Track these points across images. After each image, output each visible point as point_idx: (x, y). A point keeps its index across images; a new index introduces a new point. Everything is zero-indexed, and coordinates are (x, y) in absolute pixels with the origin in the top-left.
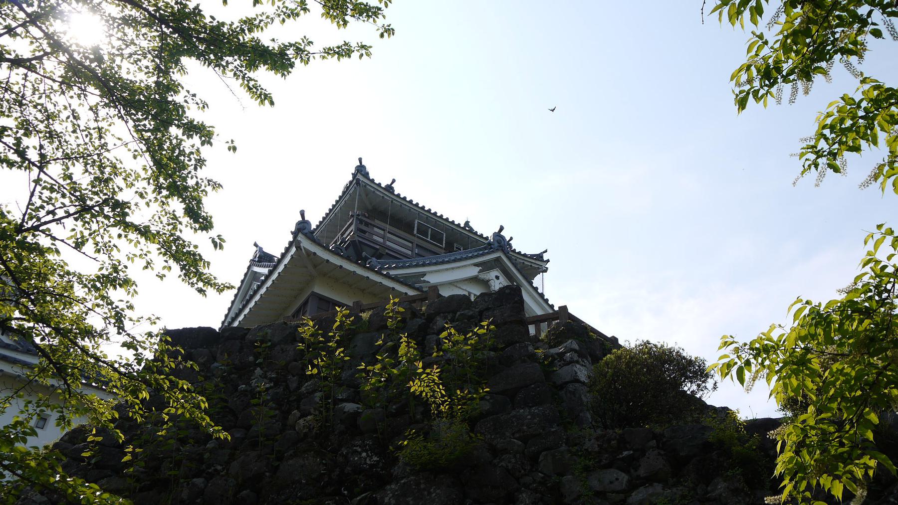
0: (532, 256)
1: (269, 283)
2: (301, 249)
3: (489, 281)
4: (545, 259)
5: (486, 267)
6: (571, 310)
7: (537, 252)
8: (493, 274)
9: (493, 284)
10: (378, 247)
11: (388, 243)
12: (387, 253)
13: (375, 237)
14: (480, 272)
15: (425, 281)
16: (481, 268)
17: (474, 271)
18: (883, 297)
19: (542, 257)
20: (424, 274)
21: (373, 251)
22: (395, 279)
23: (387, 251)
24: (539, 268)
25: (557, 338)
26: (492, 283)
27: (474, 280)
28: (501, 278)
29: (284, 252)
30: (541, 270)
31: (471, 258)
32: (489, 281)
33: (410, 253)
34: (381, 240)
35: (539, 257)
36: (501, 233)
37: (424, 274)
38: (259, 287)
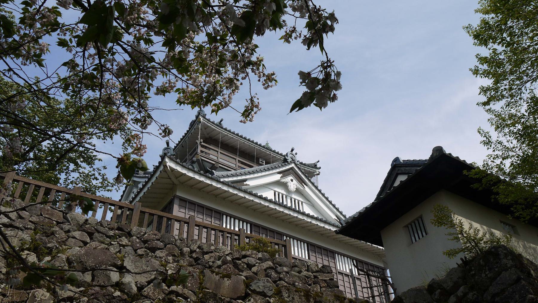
0: (308, 166)
1: (145, 190)
2: (167, 167)
3: (286, 183)
4: (318, 166)
5: (285, 173)
6: (404, 157)
7: (312, 161)
8: (288, 179)
9: (289, 185)
10: (214, 163)
11: (220, 160)
12: (220, 167)
13: (211, 156)
14: (282, 177)
15: (246, 185)
16: (282, 175)
17: (278, 177)
18: (16, 255)
19: (316, 165)
20: (245, 180)
21: (211, 165)
22: (223, 183)
23: (202, 158)
24: (314, 172)
25: (506, 255)
26: (289, 184)
27: (278, 183)
28: (294, 180)
29: (269, 199)
30: (315, 174)
31: (276, 168)
32: (286, 183)
33: (234, 166)
34: (216, 158)
35: (315, 166)
36: (255, 49)
37: (245, 180)
38: (139, 193)
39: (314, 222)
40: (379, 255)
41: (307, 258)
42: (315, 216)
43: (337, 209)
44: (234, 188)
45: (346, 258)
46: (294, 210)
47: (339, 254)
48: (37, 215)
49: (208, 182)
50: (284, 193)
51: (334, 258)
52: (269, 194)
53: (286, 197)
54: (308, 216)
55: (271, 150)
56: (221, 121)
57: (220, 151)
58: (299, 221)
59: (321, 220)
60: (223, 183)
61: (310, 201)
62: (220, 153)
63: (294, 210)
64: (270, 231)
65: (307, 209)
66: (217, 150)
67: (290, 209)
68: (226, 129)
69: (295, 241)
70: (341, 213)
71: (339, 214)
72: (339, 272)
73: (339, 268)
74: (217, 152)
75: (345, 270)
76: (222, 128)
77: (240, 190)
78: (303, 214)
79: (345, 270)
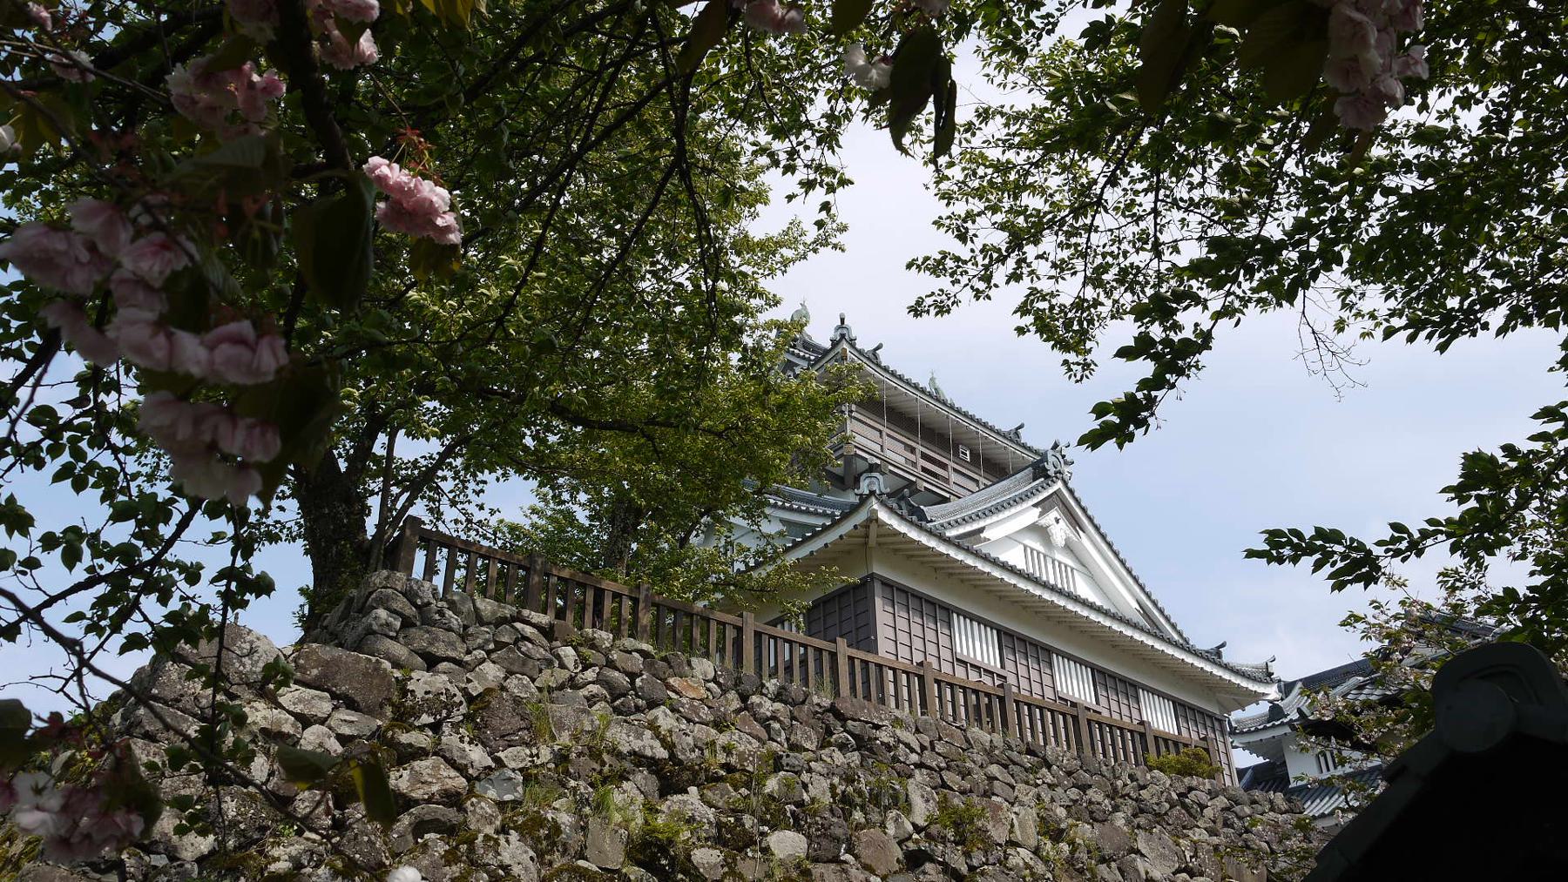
5: (1045, 506)
10: (914, 479)
11: (889, 454)
14: (1041, 514)
20: (981, 530)
34: (877, 448)
37: (981, 530)
39: (1094, 617)
40: (1210, 688)
41: (999, 666)
42: (1098, 603)
43: (1142, 588)
44: (959, 547)
45: (1072, 663)
46: (1060, 592)
47: (1060, 653)
48: (1043, 813)
49: (914, 534)
50: (1041, 549)
51: (950, 625)
52: (1014, 557)
53: (1045, 556)
54: (1085, 603)
55: (944, 403)
56: (879, 347)
57: (886, 430)
58: (889, 535)
59: (1106, 613)
60: (948, 541)
61: (1085, 562)
62: (955, 470)
63: (1060, 592)
64: (913, 595)
65: (1084, 590)
66: (881, 428)
67: (1053, 589)
68: (886, 369)
69: (975, 624)
70: (1148, 595)
71: (1143, 597)
72: (958, 660)
73: (959, 650)
74: (880, 432)
75: (972, 655)
76: (878, 365)
77: (968, 551)
78: (1076, 599)
79: (972, 655)
